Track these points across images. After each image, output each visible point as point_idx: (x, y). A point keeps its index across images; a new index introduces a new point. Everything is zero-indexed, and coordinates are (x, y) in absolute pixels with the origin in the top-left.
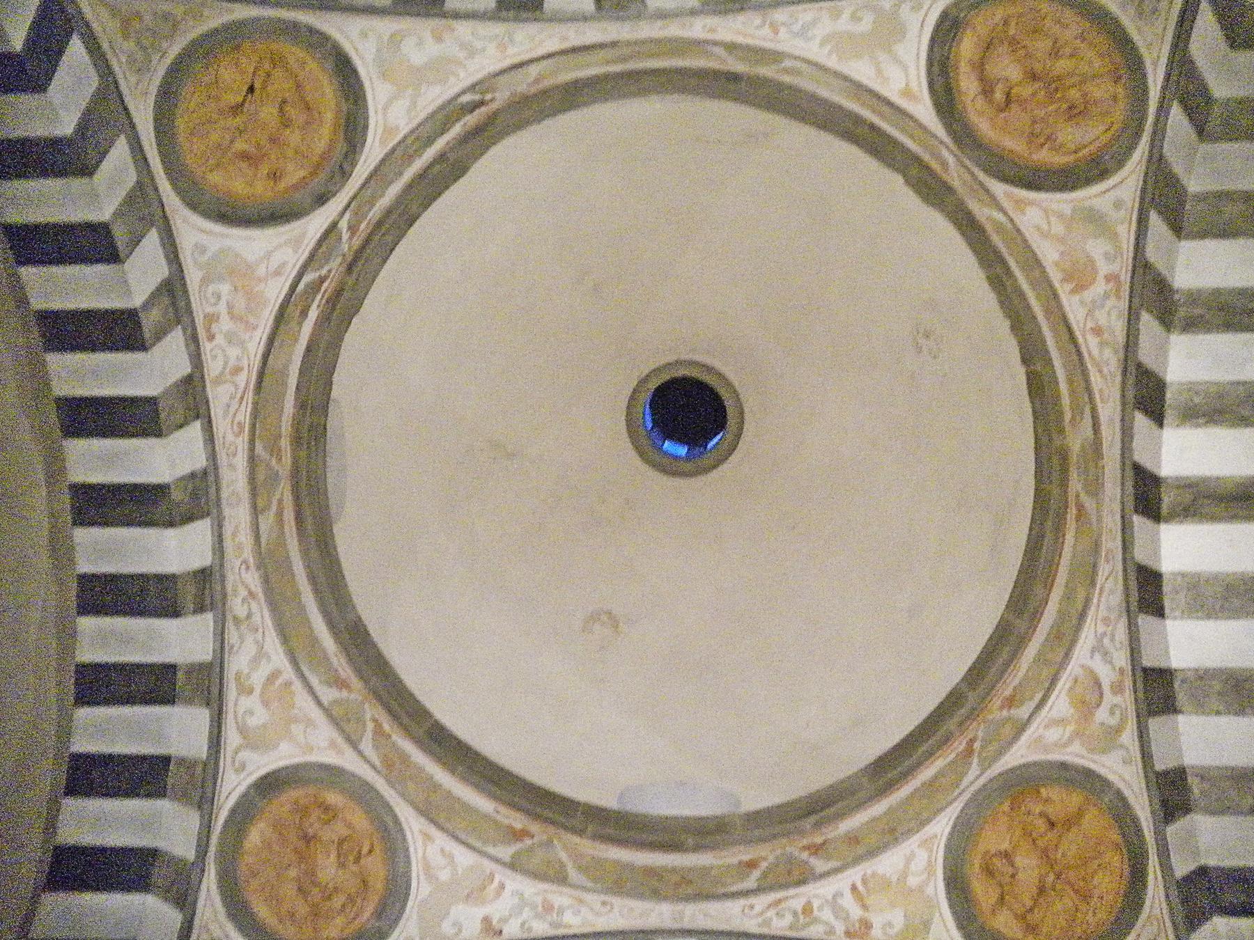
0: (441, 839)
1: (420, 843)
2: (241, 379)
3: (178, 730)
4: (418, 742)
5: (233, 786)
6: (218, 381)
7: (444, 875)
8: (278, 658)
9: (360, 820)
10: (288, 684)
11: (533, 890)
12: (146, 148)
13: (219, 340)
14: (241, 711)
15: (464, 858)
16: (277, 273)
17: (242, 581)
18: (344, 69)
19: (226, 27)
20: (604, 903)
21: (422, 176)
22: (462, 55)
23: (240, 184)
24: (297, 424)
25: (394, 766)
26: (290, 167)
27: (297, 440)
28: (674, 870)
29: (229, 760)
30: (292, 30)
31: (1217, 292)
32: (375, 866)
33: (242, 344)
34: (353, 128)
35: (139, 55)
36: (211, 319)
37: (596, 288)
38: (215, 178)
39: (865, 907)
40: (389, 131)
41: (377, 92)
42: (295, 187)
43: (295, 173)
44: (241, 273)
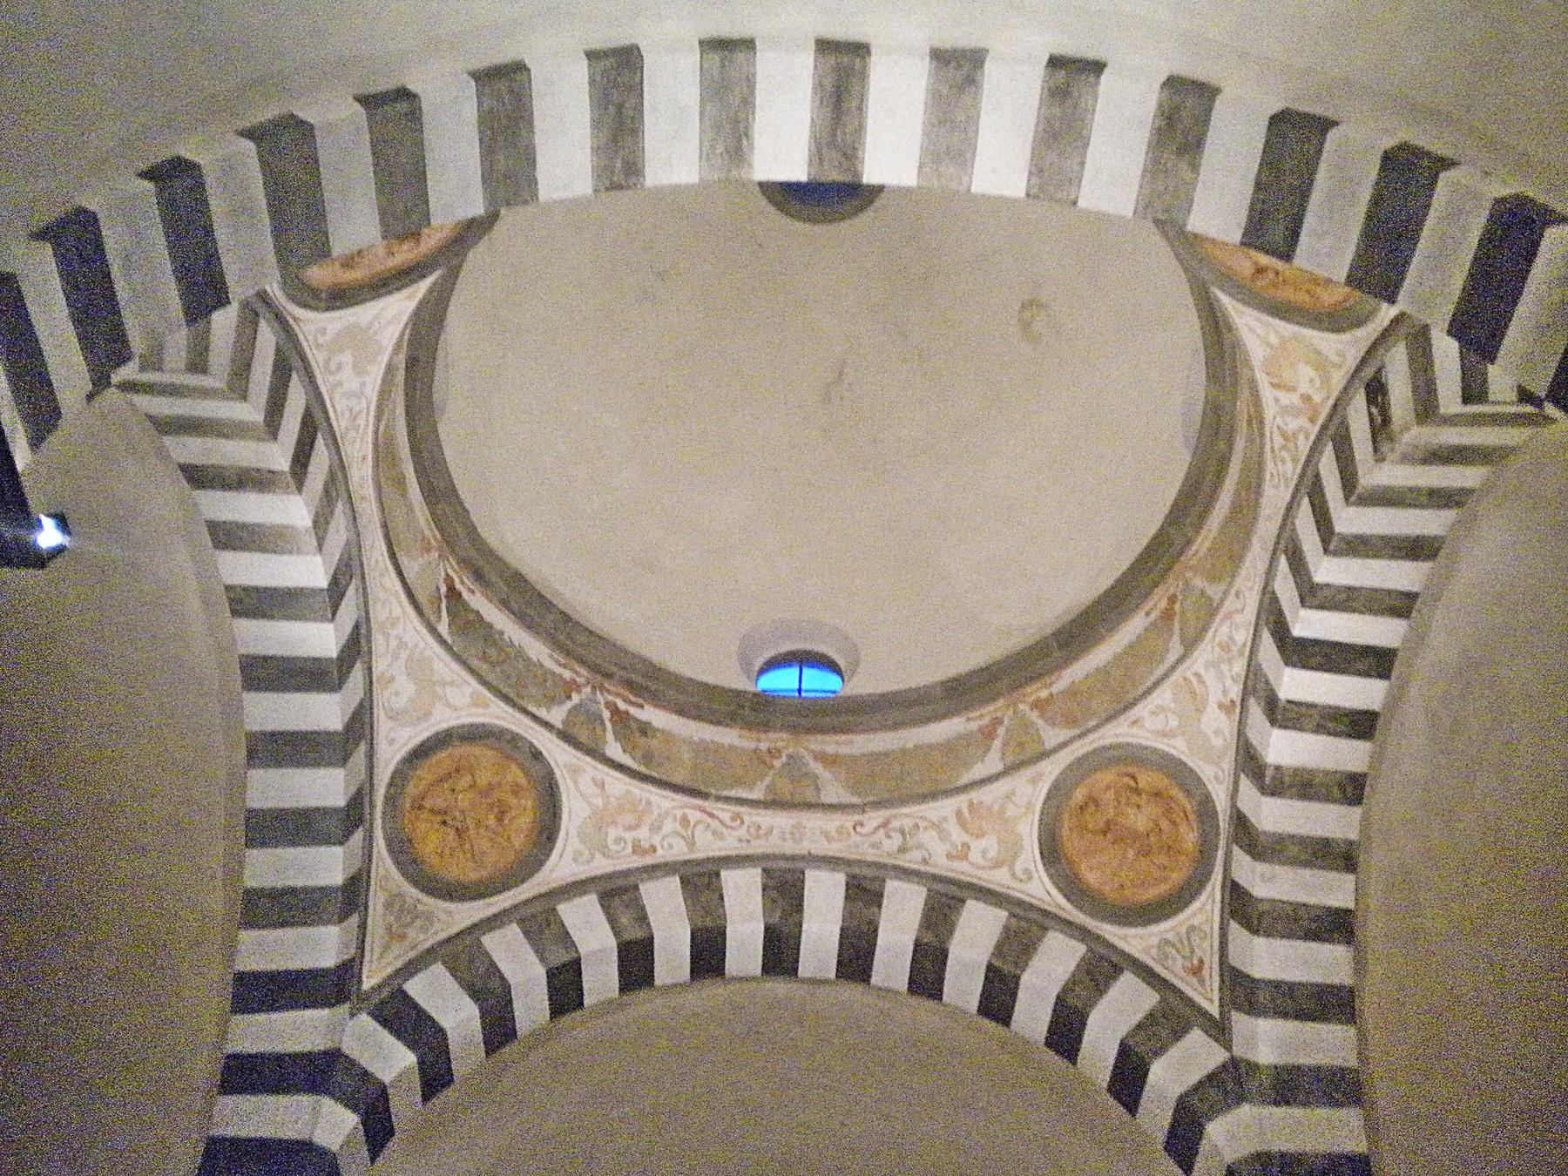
0: (1142, 710)
1: (1141, 732)
2: (694, 815)
3: (975, 937)
4: (1069, 660)
5: (1041, 889)
6: (691, 843)
7: (1174, 722)
8: (944, 809)
9: (1106, 777)
10: (971, 805)
11: (1209, 648)
12: (489, 912)
13: (656, 840)
14: (981, 862)
15: (1163, 695)
16: (602, 785)
17: (868, 836)
18: (420, 753)
19: (391, 851)
20: (1237, 595)
21: (521, 618)
22: (404, 655)
23: (524, 818)
24: (749, 725)
25: (1075, 712)
26: (509, 778)
27: (765, 726)
28: (1237, 492)
29: (1018, 885)
30: (391, 800)
31: (596, 150)
32: (1146, 779)
33: (663, 816)
34: (474, 734)
35: (418, 923)
36: (637, 849)
37: (661, 275)
38: (518, 841)
39: (1293, 389)
40: (477, 702)
41: (443, 719)
42: (527, 774)
43: (515, 774)
44: (600, 821)
